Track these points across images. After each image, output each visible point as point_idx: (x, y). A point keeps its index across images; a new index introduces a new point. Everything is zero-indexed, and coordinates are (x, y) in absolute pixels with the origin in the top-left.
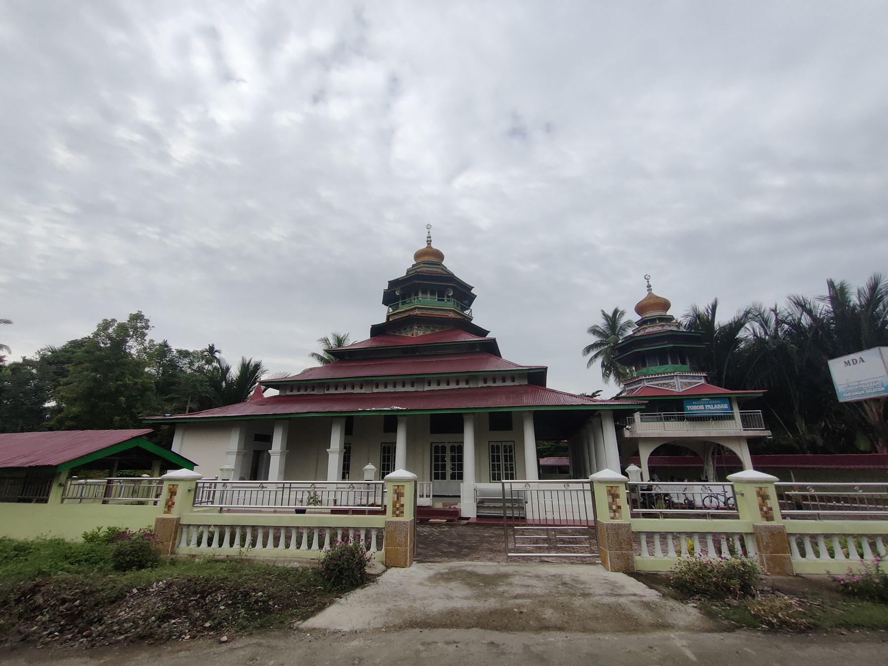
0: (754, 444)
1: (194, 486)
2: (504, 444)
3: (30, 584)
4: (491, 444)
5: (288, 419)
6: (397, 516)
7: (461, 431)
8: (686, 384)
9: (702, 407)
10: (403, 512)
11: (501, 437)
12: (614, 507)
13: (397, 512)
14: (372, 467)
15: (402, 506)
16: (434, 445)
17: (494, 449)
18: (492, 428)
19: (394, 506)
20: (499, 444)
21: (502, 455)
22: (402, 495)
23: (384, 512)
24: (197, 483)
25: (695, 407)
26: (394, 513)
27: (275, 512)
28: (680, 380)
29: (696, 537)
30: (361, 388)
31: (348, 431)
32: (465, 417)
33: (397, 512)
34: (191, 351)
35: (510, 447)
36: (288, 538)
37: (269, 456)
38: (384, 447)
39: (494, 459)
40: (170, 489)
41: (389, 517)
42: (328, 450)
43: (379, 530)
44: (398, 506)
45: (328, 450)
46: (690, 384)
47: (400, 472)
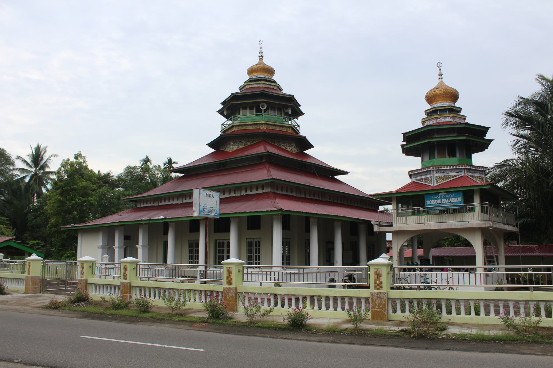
0: (489, 236)
1: (241, 269)
2: (255, 240)
3: (161, 317)
4: (248, 240)
5: (175, 222)
6: (378, 289)
7: (229, 231)
8: (441, 178)
9: (439, 201)
10: (382, 287)
11: (254, 234)
12: (378, 282)
13: (378, 287)
14: (107, 256)
15: (381, 283)
16: (218, 242)
17: (250, 244)
18: (216, 231)
19: (375, 283)
20: (224, 241)
21: (254, 248)
22: (231, 273)
23: (368, 287)
24: (137, 265)
25: (433, 202)
26: (375, 287)
27: (156, 281)
28: (436, 174)
29: (192, 292)
30: (263, 189)
31: (286, 227)
32: (201, 222)
33: (378, 287)
34: (109, 162)
35: (259, 242)
36: (335, 303)
37: (137, 249)
38: (249, 242)
39: (250, 251)
40: (228, 270)
41: (372, 290)
42: (137, 246)
43: (367, 299)
44: (378, 282)
45: (137, 246)
46: (447, 177)
47: (233, 260)
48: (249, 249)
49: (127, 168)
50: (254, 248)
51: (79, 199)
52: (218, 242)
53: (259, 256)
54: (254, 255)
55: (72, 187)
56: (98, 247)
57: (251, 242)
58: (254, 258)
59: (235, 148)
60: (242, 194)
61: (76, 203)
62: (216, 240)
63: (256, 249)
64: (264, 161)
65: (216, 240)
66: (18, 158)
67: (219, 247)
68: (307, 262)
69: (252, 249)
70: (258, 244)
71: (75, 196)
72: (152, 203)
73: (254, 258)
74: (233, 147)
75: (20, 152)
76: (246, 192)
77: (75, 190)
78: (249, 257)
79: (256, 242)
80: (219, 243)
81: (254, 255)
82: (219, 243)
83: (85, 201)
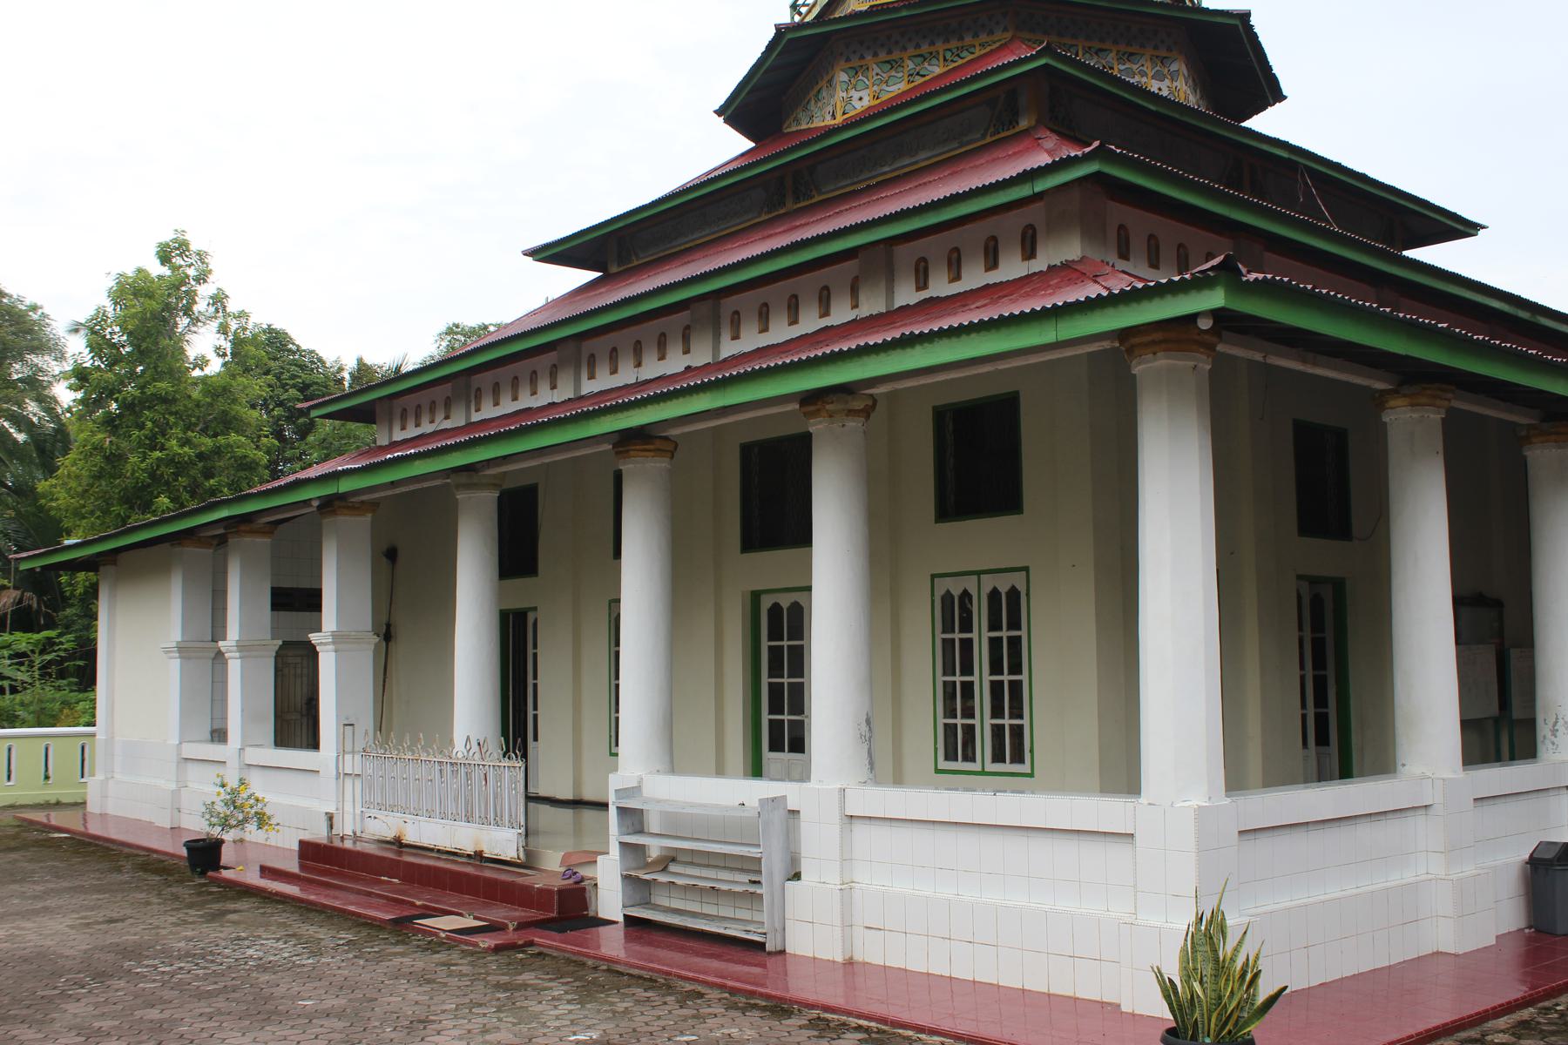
2: (988, 583)
16: (766, 603)
17: (955, 612)
21: (981, 637)
35: (1014, 594)
38: (947, 598)
48: (948, 645)
49: (450, 331)
50: (981, 637)
51: (185, 442)
52: (766, 603)
53: (1015, 643)
54: (982, 678)
55: (150, 390)
56: (167, 651)
57: (998, 757)
58: (983, 700)
59: (862, 100)
60: (900, 301)
61: (171, 461)
62: (756, 596)
63: (995, 644)
64: (1024, 124)
65: (756, 596)
66: (76, 331)
67: (775, 634)
68: (1121, 771)
69: (967, 645)
70: (1008, 609)
71: (163, 429)
72: (440, 416)
73: (983, 700)
74: (850, 98)
75: (70, 296)
76: (922, 285)
77: (165, 400)
78: (949, 690)
79: (994, 595)
80: (775, 610)
81: (982, 678)
82: (775, 610)
83: (217, 452)
